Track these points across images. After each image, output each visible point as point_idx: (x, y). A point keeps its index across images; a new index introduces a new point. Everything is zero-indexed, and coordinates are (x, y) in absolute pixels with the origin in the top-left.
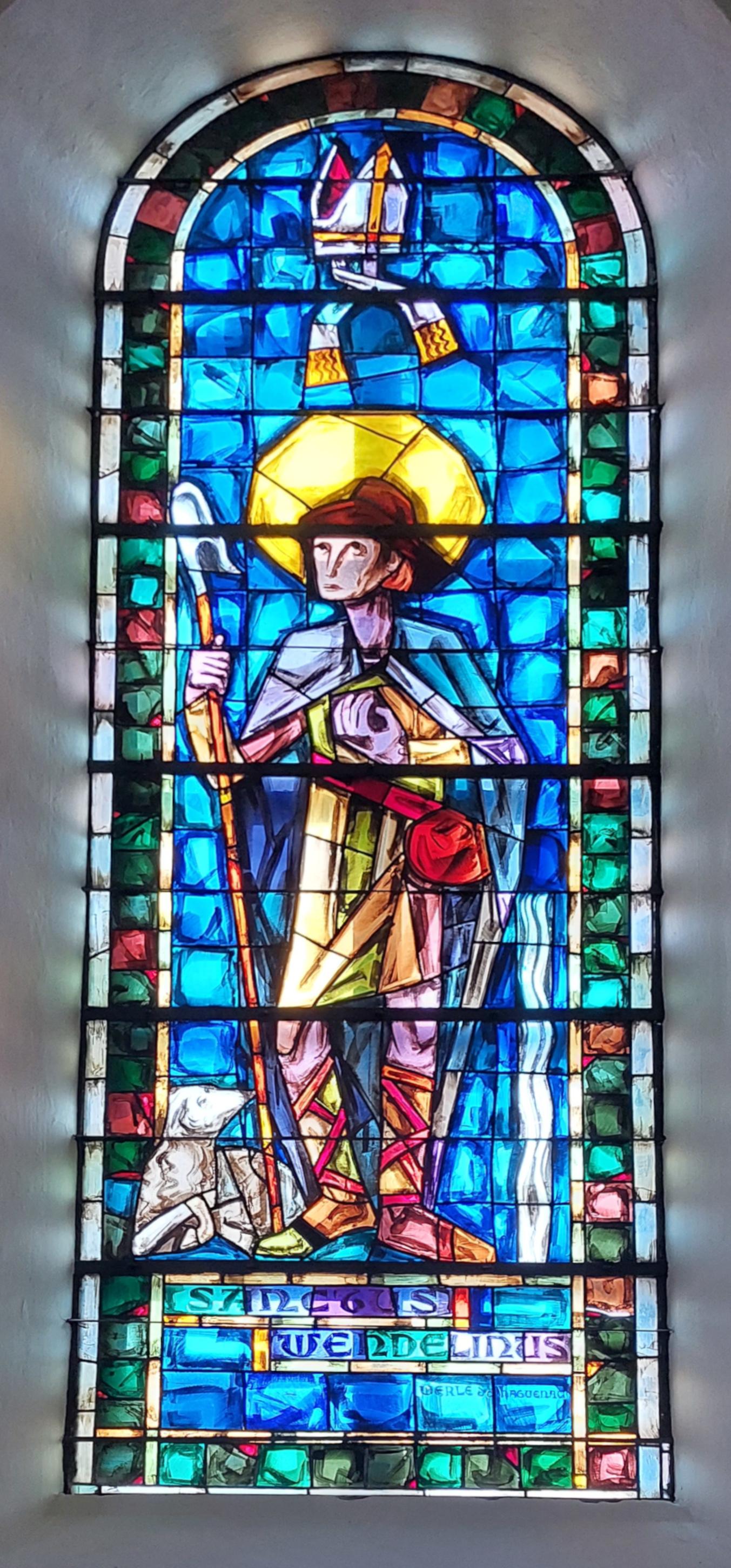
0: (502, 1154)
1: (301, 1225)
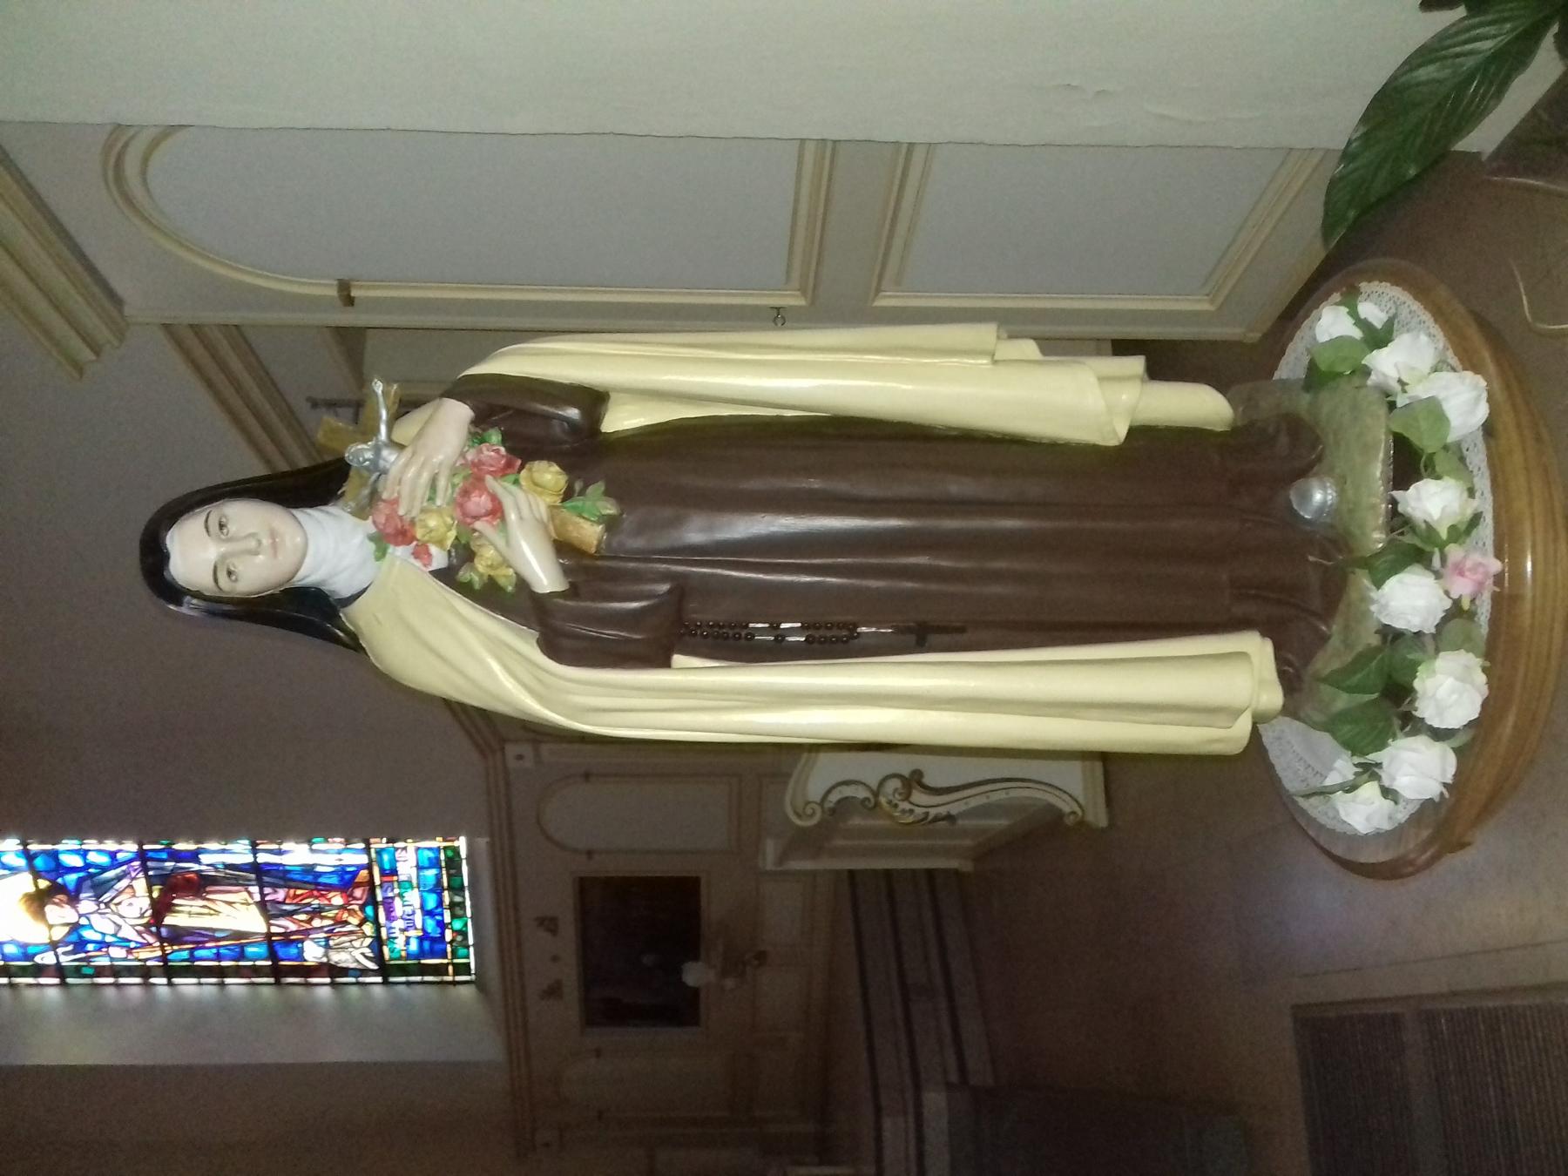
0: (319, 869)
1: (360, 925)
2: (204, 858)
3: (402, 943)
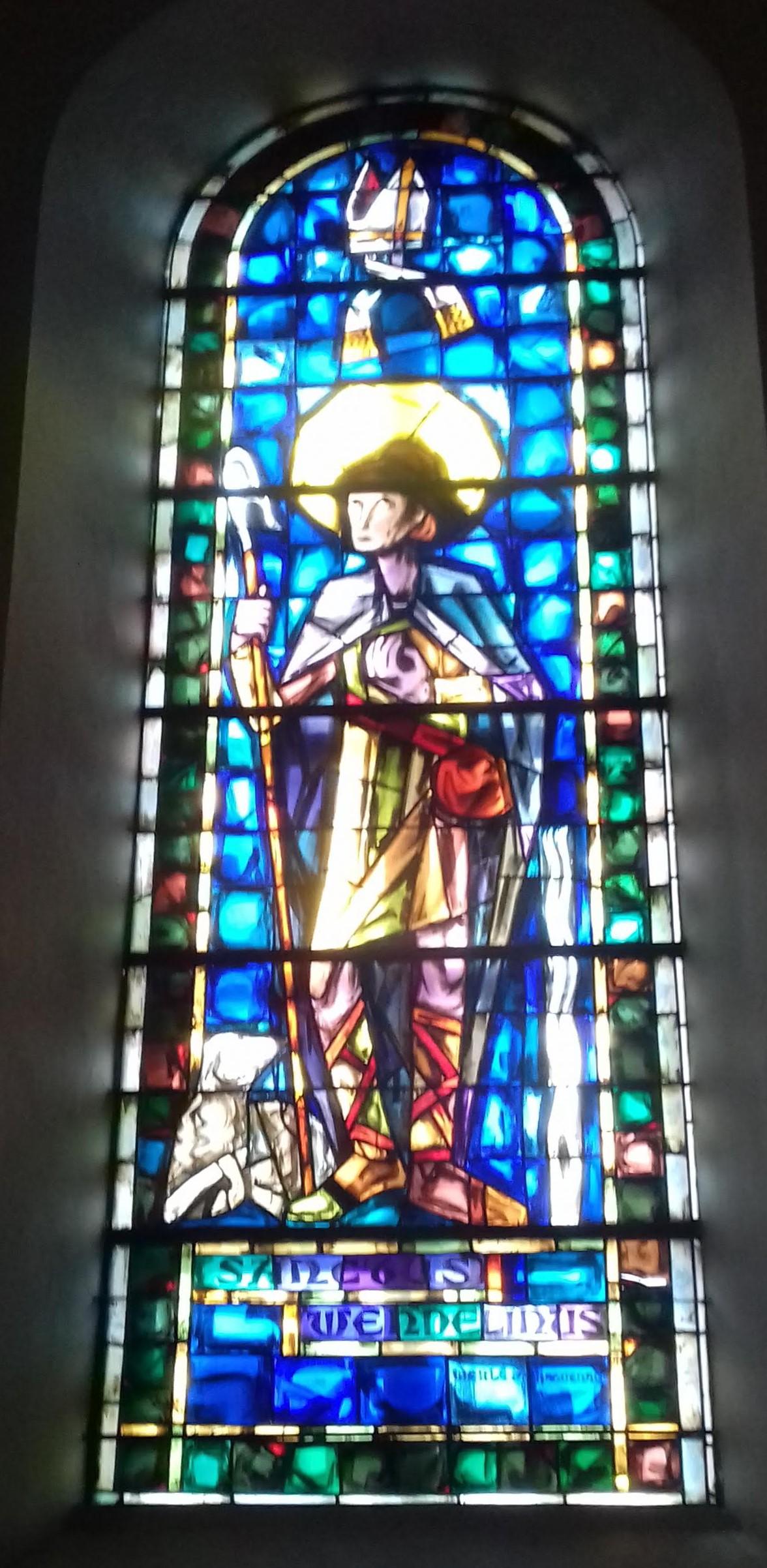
0: (532, 1103)
1: (332, 1186)
2: (557, 842)
3: (564, 1211)
